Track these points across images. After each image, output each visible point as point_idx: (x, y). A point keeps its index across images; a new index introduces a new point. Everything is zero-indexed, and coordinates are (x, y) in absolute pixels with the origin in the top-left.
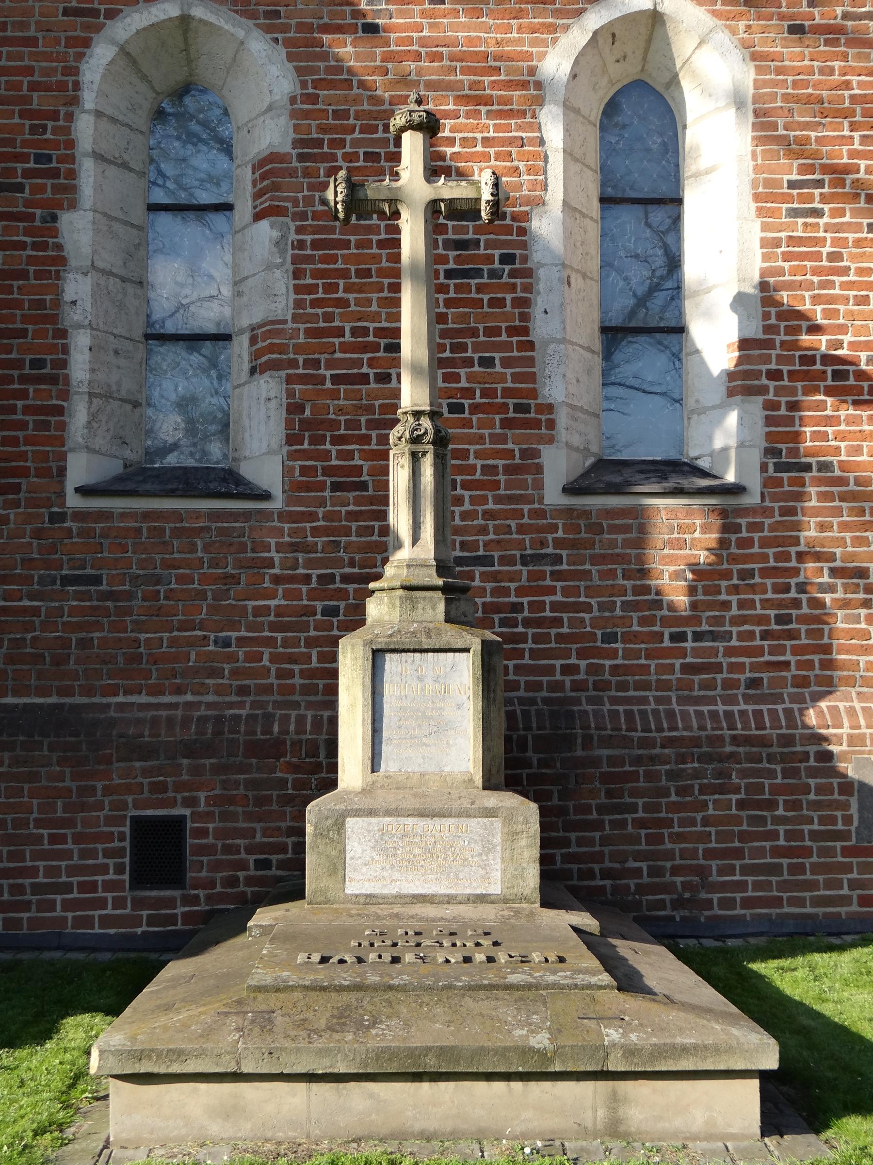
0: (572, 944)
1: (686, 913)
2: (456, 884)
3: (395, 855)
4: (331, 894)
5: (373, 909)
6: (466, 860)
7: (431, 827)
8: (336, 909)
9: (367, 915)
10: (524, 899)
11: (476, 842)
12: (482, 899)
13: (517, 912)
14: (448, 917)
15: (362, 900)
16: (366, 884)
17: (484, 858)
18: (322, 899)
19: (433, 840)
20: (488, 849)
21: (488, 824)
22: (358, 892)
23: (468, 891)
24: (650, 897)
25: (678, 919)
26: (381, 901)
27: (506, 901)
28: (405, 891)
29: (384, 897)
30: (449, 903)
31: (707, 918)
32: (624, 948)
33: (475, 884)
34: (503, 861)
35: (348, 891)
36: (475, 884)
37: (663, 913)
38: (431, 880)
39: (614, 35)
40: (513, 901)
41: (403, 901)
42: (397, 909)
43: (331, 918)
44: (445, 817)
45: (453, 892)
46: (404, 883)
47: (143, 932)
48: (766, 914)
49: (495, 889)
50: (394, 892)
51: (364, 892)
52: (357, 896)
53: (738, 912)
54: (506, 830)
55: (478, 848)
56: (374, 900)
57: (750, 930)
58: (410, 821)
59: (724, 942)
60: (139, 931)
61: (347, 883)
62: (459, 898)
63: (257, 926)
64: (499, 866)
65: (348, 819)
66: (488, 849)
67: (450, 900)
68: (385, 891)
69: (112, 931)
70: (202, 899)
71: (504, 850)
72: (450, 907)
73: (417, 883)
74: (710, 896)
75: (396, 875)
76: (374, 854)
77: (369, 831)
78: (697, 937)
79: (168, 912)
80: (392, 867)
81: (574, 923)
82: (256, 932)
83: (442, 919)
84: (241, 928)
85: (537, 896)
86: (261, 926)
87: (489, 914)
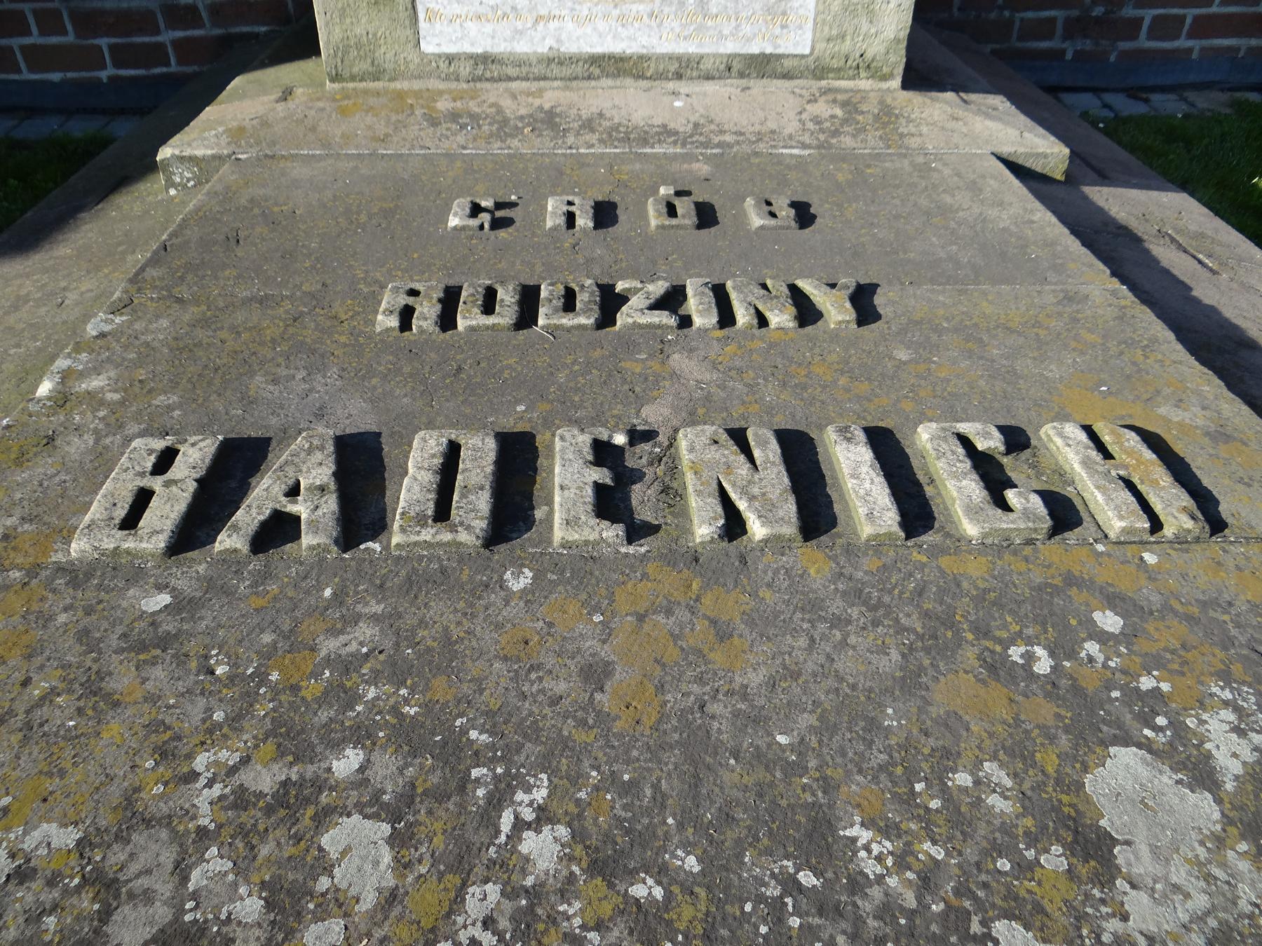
1: (1088, 45)
2: (700, 28)
4: (386, 55)
5: (494, 94)
8: (400, 96)
9: (474, 117)
10: (868, 67)
12: (761, 66)
13: (851, 105)
14: (679, 125)
15: (465, 69)
16: (472, 26)
18: (365, 66)
23: (730, 47)
24: (1030, 15)
25: (1069, 56)
26: (511, 71)
27: (819, 71)
29: (520, 62)
30: (679, 76)
31: (1124, 54)
32: (1120, 203)
33: (747, 29)
35: (428, 47)
36: (747, 29)
37: (1044, 45)
38: (639, 18)
40: (839, 73)
41: (566, 71)
42: (552, 96)
43: (381, 129)
46: (570, 26)
47: (110, 78)
48: (1229, 48)
49: (797, 41)
50: (543, 49)
51: (469, 49)
52: (451, 58)
53: (1182, 43)
56: (495, 70)
57: (1192, 78)
59: (1146, 101)
60: (104, 75)
61: (423, 25)
62: (707, 65)
63: (181, 159)
67: (684, 68)
68: (522, 47)
69: (56, 77)
70: (204, 15)
72: (683, 87)
73: (601, 25)
74: (1139, 12)
78: (1096, 91)
79: (147, 39)
81: (1006, 150)
82: (182, 174)
83: (666, 132)
84: (146, 166)
85: (898, 60)
86: (191, 159)
87: (779, 111)
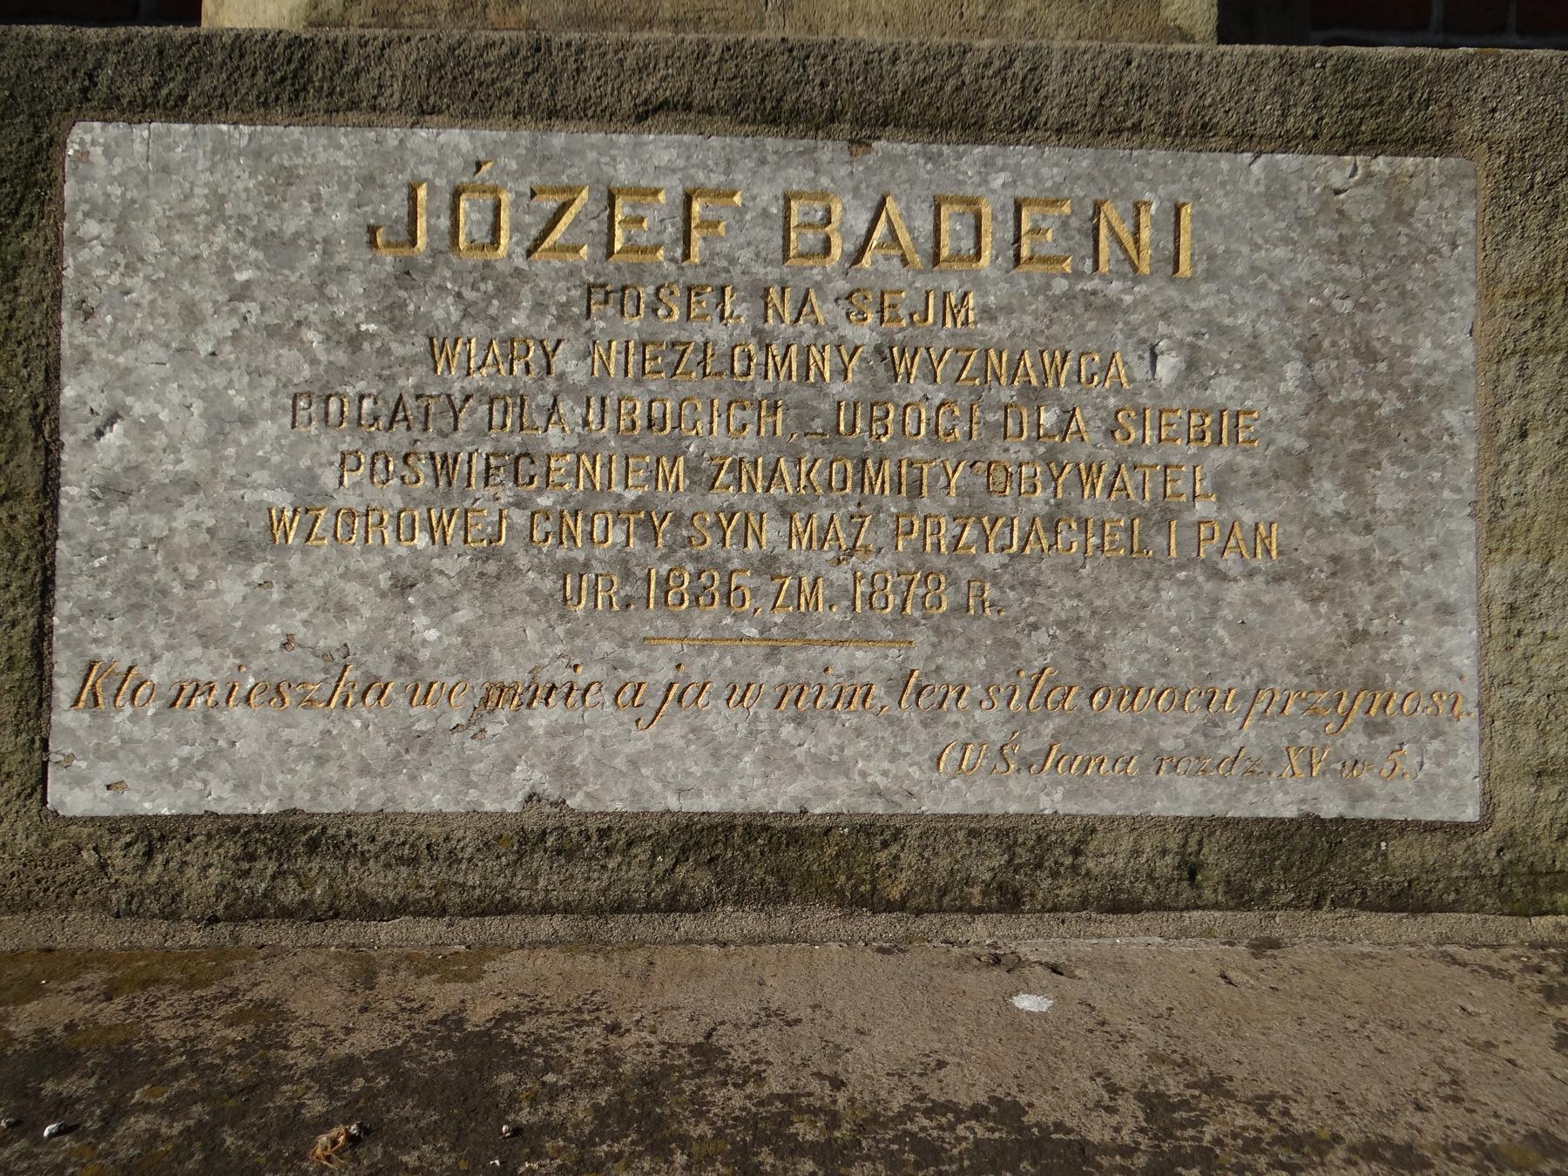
0: (1556, 62)
3: (518, 464)
6: (1165, 514)
7: (850, 216)
11: (1256, 361)
12: (1309, 866)
15: (204, 875)
17: (1330, 497)
19: (865, 334)
20: (1361, 427)
21: (1363, 205)
22: (162, 805)
23: (1186, 797)
26: (377, 881)
28: (606, 795)
29: (413, 845)
30: (1009, 900)
33: (1246, 735)
34: (1497, 527)
35: (75, 796)
38: (854, 694)
39: (1509, 1061)
41: (587, 881)
44: (973, 128)
45: (1053, 801)
46: (602, 716)
49: (1437, 779)
50: (501, 801)
51: (224, 798)
52: (153, 835)
54: (1521, 261)
55: (1272, 404)
56: (320, 879)
58: (661, 158)
61: (65, 717)
62: (1109, 860)
64: (1458, 575)
65: (88, 138)
66: (1361, 427)
67: (1026, 871)
68: (429, 794)
71: (1504, 436)
73: (720, 718)
75: (529, 645)
76: (322, 448)
77: (278, 247)
80: (492, 567)
